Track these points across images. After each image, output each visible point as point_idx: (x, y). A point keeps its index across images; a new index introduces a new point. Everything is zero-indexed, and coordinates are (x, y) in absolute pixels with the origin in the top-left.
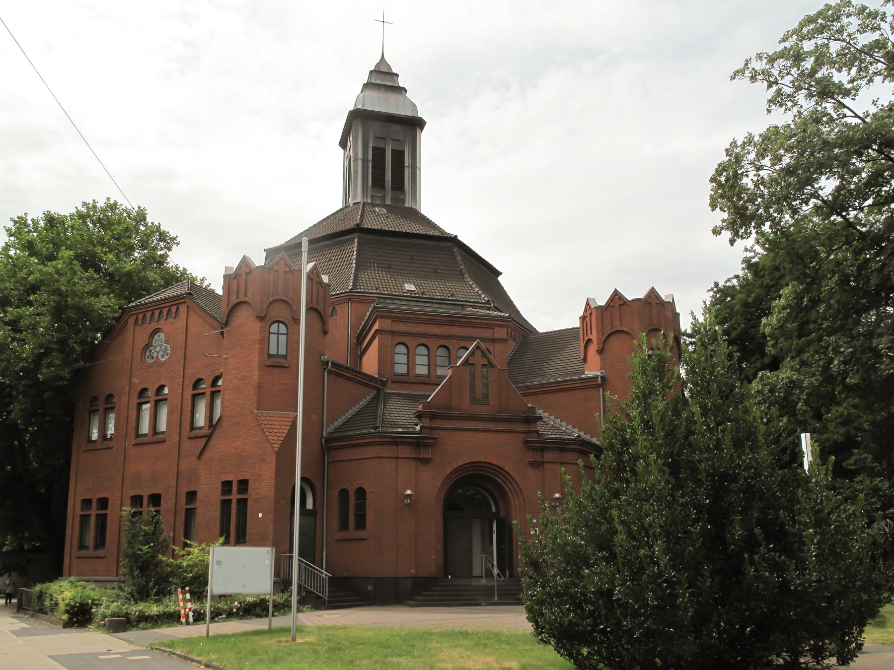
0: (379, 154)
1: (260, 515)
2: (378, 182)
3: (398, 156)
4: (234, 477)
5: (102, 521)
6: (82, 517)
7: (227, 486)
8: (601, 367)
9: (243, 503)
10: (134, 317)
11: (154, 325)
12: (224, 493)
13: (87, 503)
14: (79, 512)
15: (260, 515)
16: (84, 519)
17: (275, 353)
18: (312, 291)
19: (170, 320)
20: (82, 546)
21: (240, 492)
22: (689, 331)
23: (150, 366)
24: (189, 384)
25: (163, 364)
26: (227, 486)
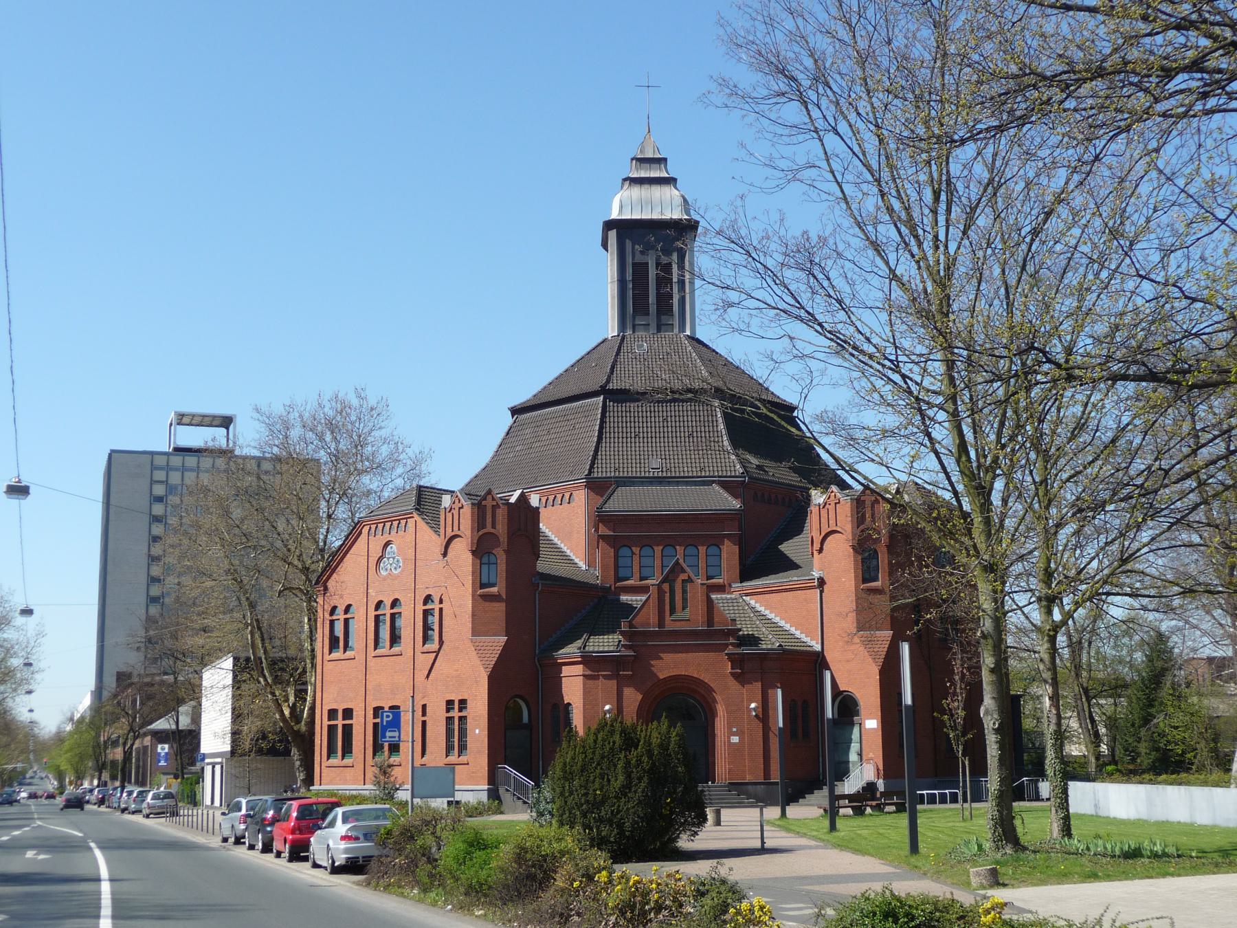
0: (640, 270)
1: (477, 731)
2: (641, 307)
3: (664, 281)
4: (456, 697)
5: (348, 730)
6: (329, 726)
7: (450, 703)
8: (858, 621)
9: (462, 719)
10: (368, 527)
11: (387, 537)
12: (448, 710)
13: (332, 714)
14: (326, 723)
15: (477, 731)
16: (332, 729)
17: (663, 322)
18: (878, 770)
19: (565, 505)
20: (331, 751)
21: (460, 710)
22: (726, 541)
23: (385, 579)
24: (420, 600)
25: (396, 577)
26: (450, 703)
